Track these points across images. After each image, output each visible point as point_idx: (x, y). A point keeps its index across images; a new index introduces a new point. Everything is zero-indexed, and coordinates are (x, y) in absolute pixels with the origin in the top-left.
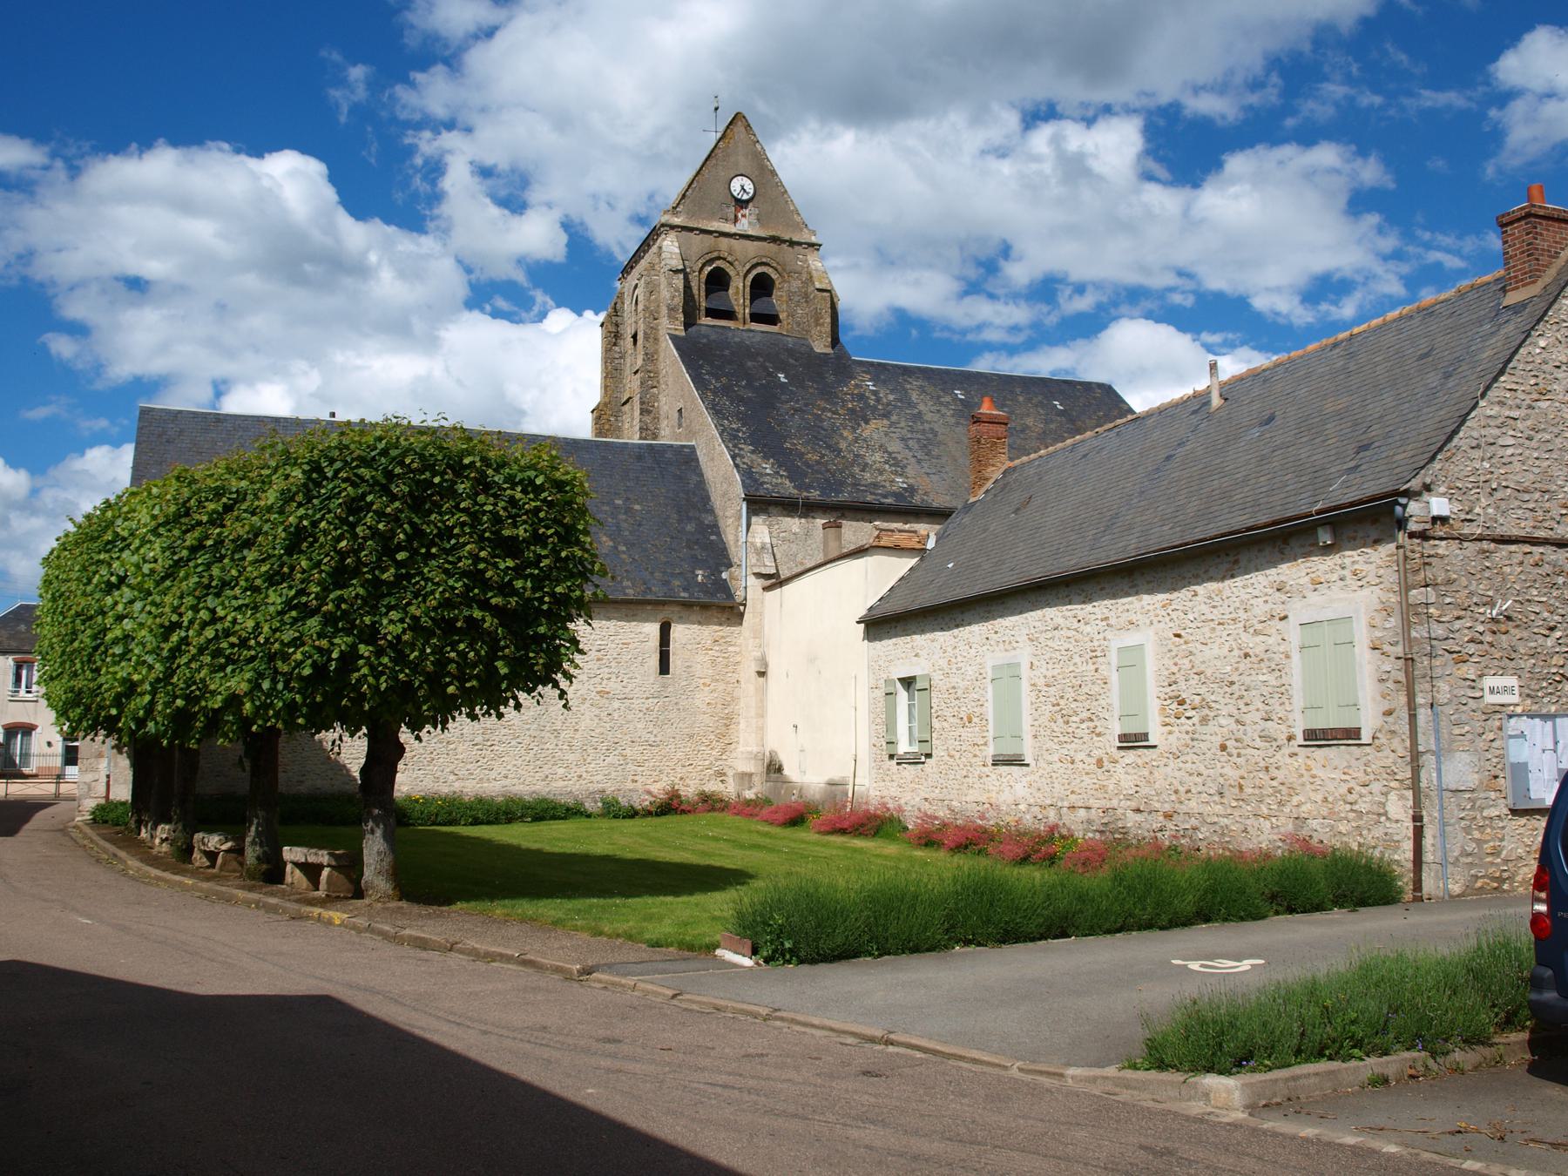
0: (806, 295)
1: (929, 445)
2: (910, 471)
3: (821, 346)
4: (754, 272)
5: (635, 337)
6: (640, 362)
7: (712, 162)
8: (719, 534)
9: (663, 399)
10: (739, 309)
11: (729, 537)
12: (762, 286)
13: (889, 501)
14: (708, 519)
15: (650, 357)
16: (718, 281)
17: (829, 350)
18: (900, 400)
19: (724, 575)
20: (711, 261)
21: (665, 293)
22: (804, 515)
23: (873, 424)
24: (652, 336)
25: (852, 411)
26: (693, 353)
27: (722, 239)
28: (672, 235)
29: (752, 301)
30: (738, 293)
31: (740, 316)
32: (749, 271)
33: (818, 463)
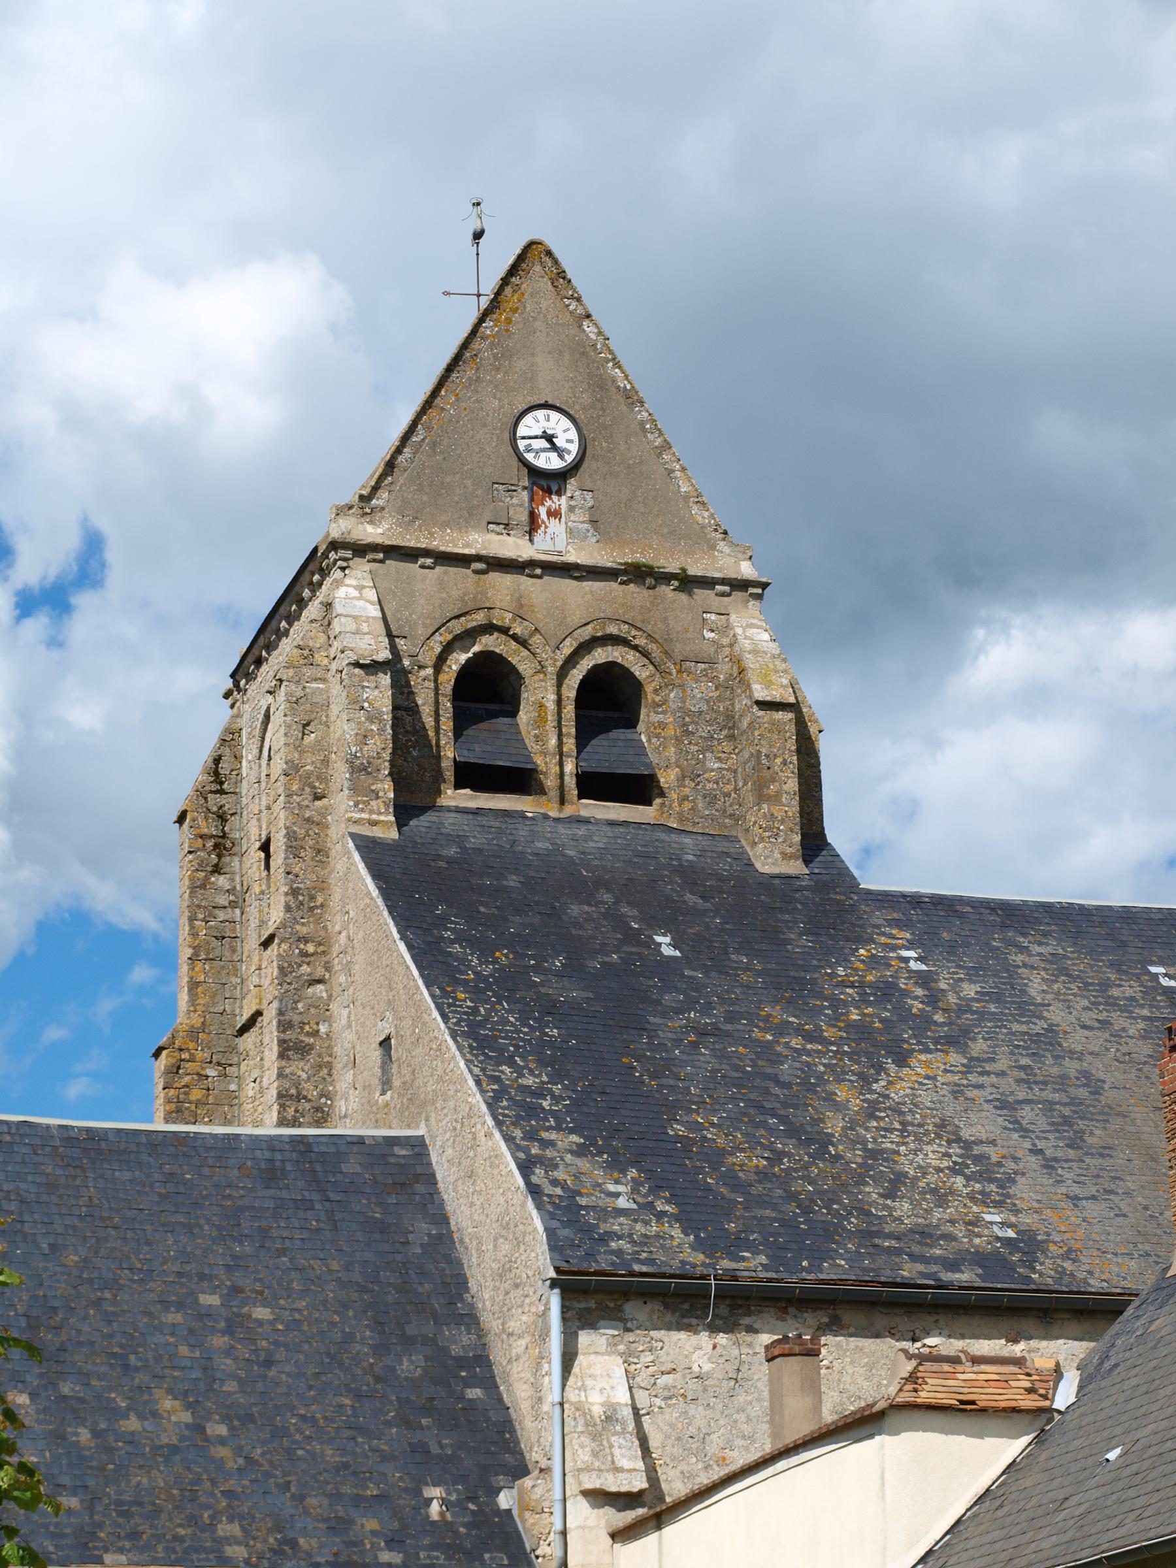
0: (730, 721)
1: (1075, 1118)
2: (1023, 1191)
3: (774, 857)
4: (586, 664)
5: (265, 847)
6: (276, 915)
7: (466, 372)
8: (490, 1383)
9: (340, 1013)
10: (546, 765)
11: (518, 1390)
12: (607, 700)
13: (965, 1276)
14: (459, 1342)
15: (306, 901)
16: (487, 689)
17: (796, 867)
18: (997, 998)
19: (505, 1500)
20: (470, 635)
21: (342, 728)
22: (724, 1324)
23: (920, 1064)
24: (307, 841)
25: (861, 1031)
26: (414, 884)
27: (495, 577)
28: (361, 570)
29: (583, 738)
30: (543, 722)
31: (550, 782)
32: (571, 661)
33: (763, 1175)
